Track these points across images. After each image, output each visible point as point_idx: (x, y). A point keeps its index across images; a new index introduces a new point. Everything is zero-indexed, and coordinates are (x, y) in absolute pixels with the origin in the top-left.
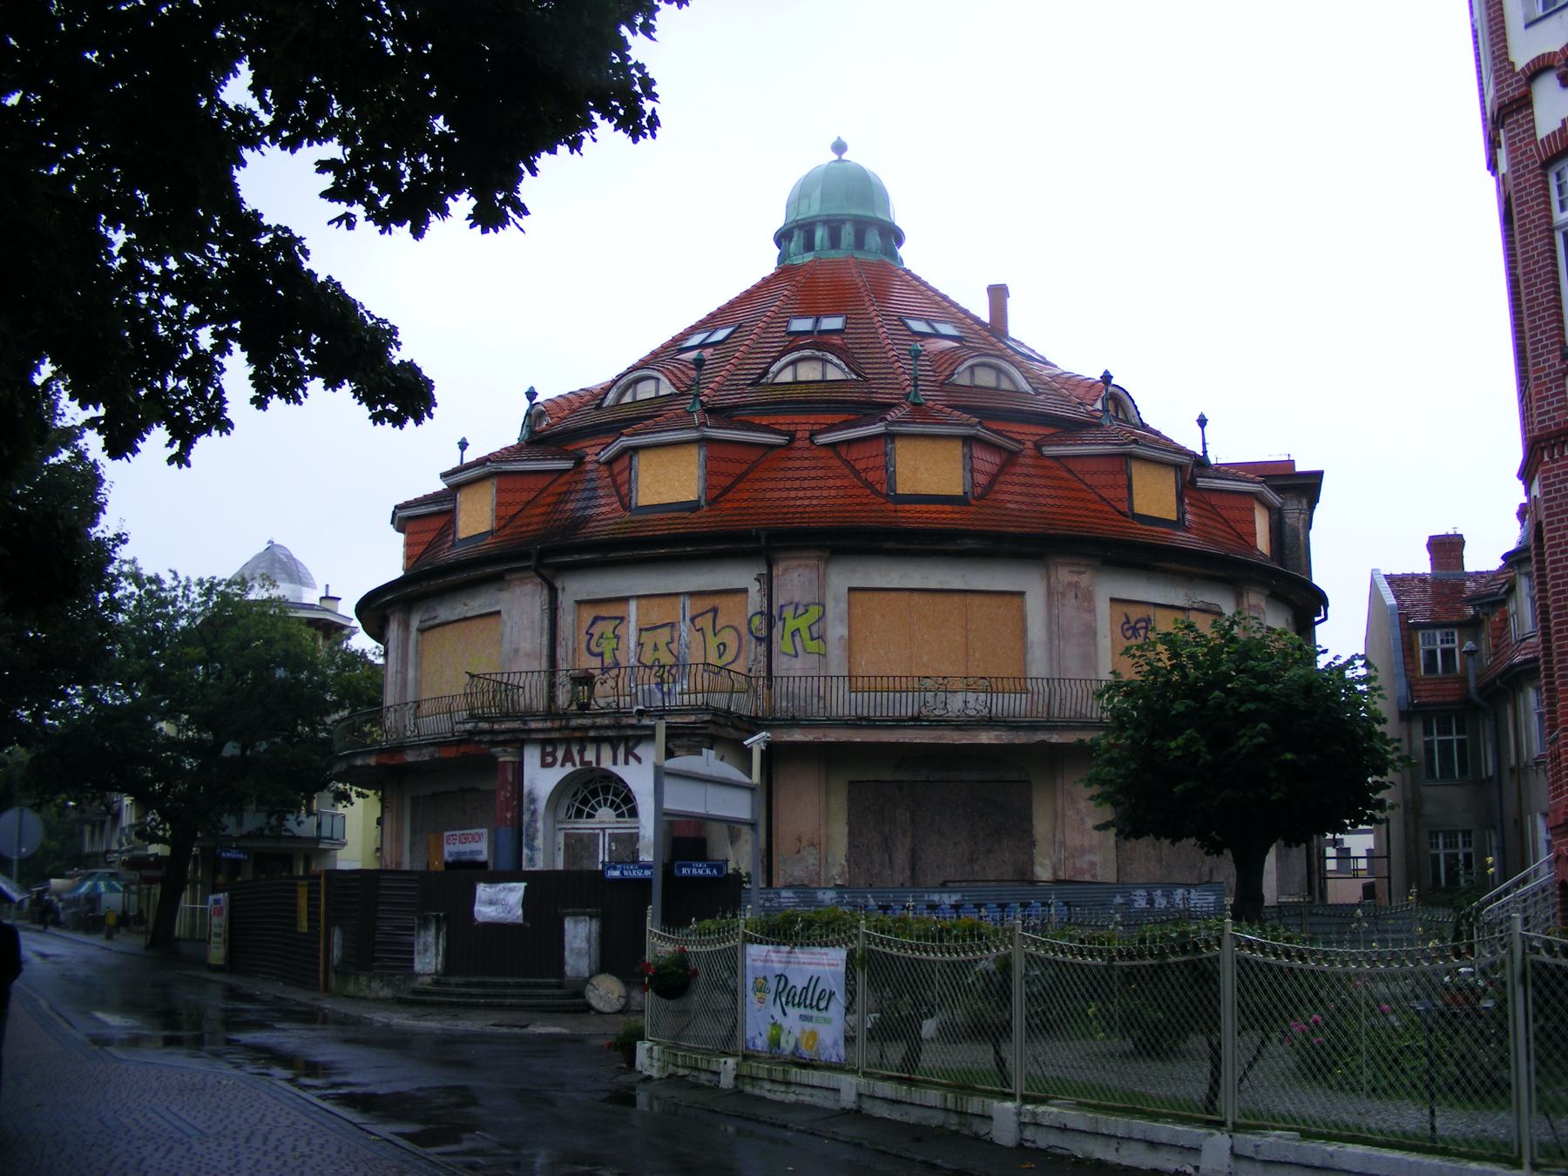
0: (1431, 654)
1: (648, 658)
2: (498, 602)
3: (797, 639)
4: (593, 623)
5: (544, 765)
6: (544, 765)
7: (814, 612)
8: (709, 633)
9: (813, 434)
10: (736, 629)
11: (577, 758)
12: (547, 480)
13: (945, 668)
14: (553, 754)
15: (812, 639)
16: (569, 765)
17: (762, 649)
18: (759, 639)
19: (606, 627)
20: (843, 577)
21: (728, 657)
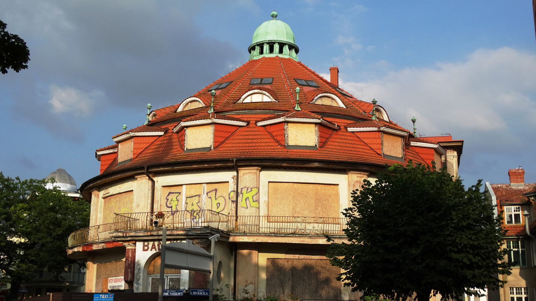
0: (511, 216)
1: (190, 208)
2: (132, 186)
3: (248, 201)
4: (169, 195)
5: (144, 250)
6: (144, 250)
7: (255, 191)
8: (213, 199)
9: (256, 122)
10: (224, 197)
12: (154, 139)
13: (306, 213)
14: (147, 246)
15: (254, 201)
16: (154, 250)
17: (235, 205)
18: (232, 201)
19: (173, 197)
20: (267, 176)
21: (221, 208)
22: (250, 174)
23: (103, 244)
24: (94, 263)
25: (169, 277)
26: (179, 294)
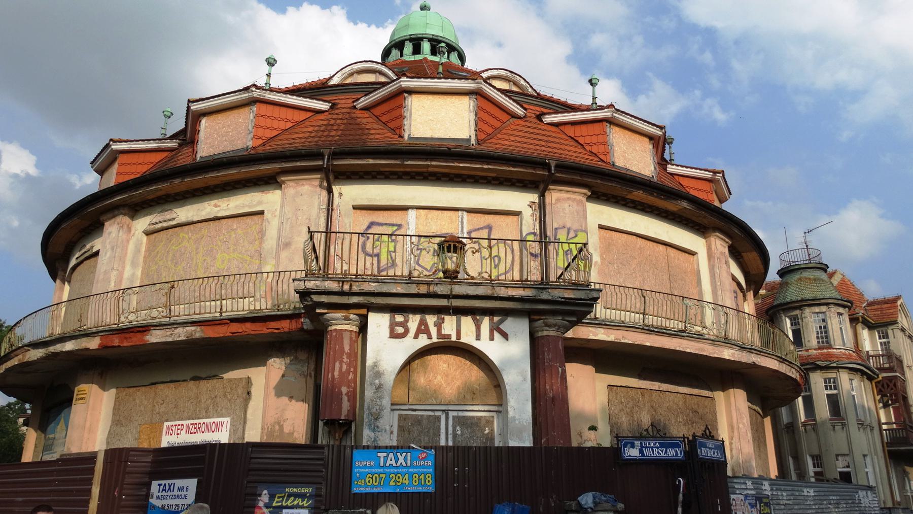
2: (260, 203)
5: (393, 335)
6: (393, 335)
11: (433, 331)
12: (301, 116)
14: (404, 324)
22: (570, 202)
23: (190, 329)
24: (104, 388)
25: (451, 414)
26: (671, 452)
